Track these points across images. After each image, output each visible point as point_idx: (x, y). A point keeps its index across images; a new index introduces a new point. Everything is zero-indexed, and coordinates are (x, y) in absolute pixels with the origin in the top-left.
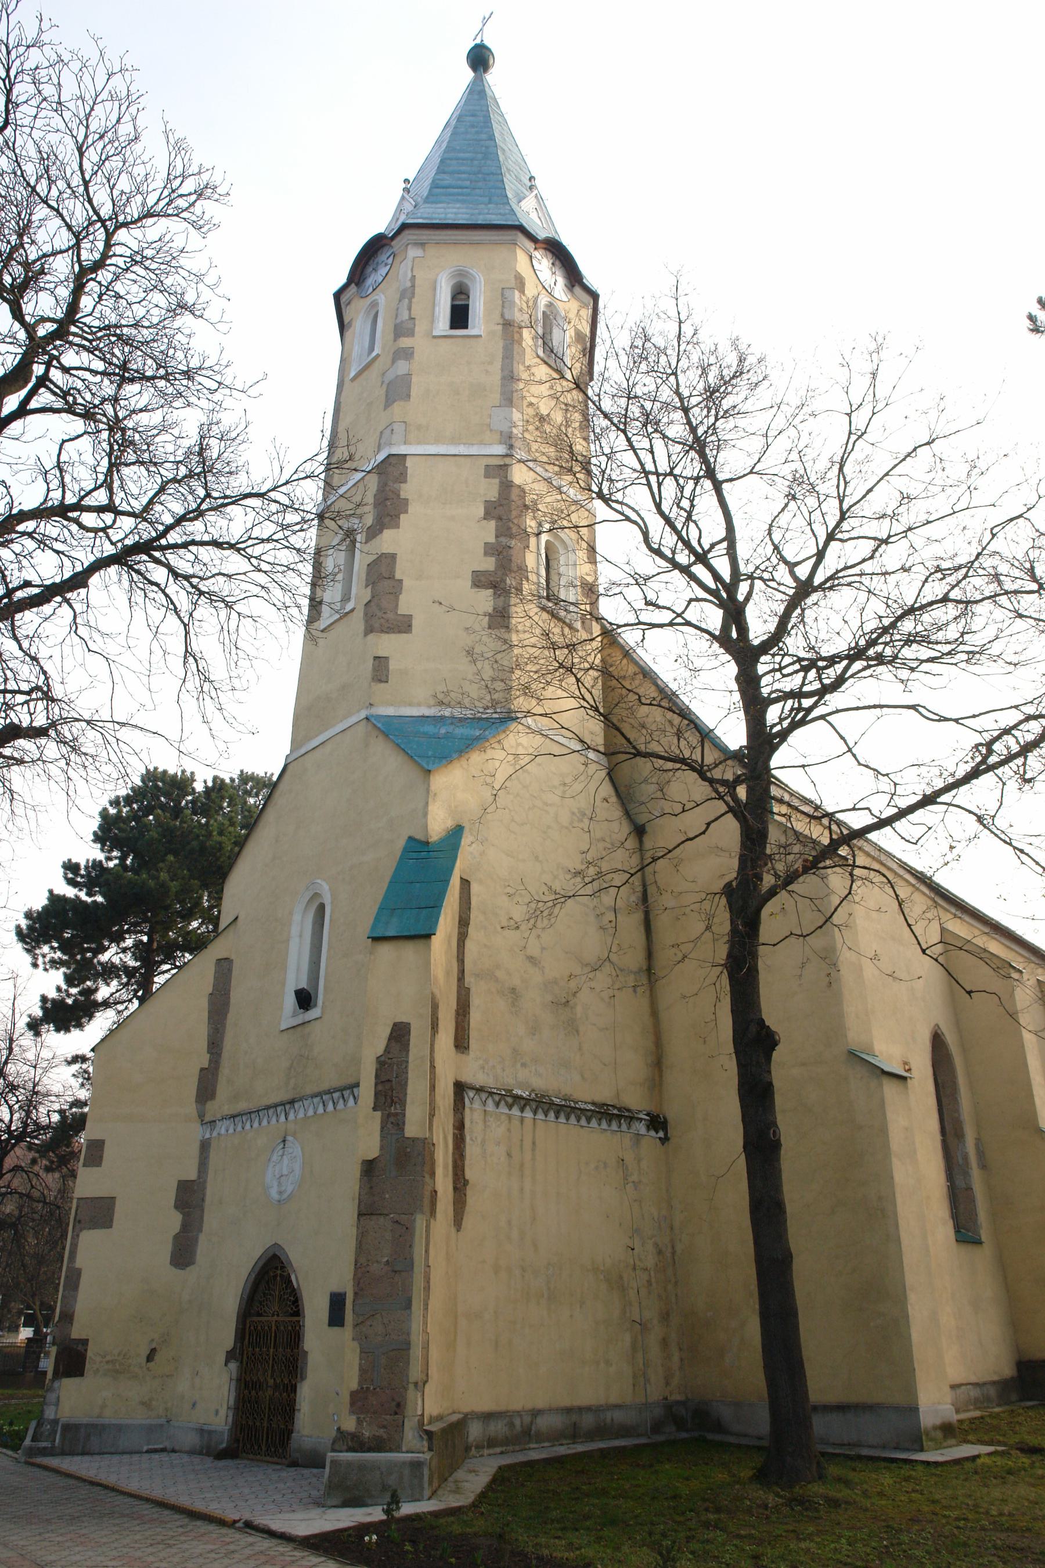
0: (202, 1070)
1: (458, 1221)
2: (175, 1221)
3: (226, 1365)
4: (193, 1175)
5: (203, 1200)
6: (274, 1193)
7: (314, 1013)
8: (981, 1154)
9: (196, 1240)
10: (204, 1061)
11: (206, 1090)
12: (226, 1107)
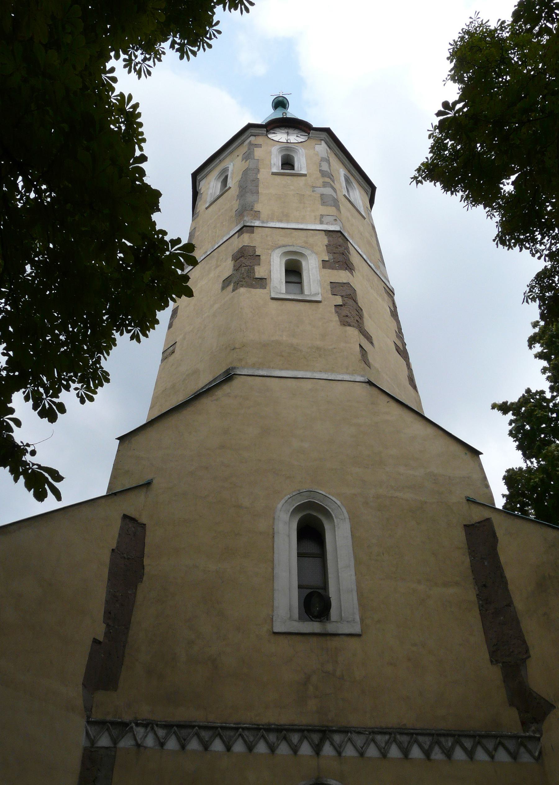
11: (105, 666)
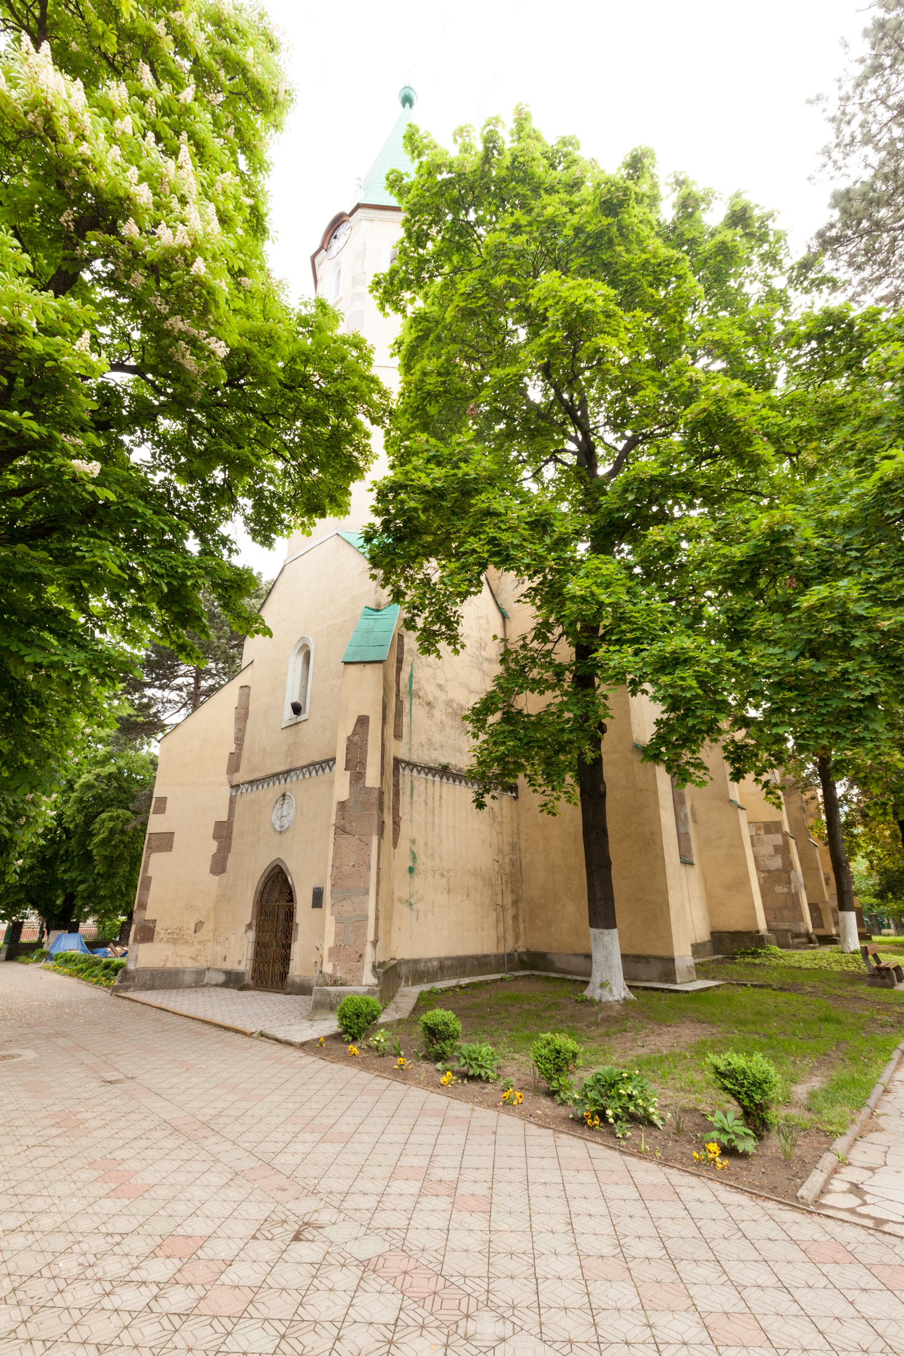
1: (395, 845)
2: (213, 846)
4: (225, 819)
7: (302, 717)
8: (693, 814)
10: (233, 748)
11: (234, 764)
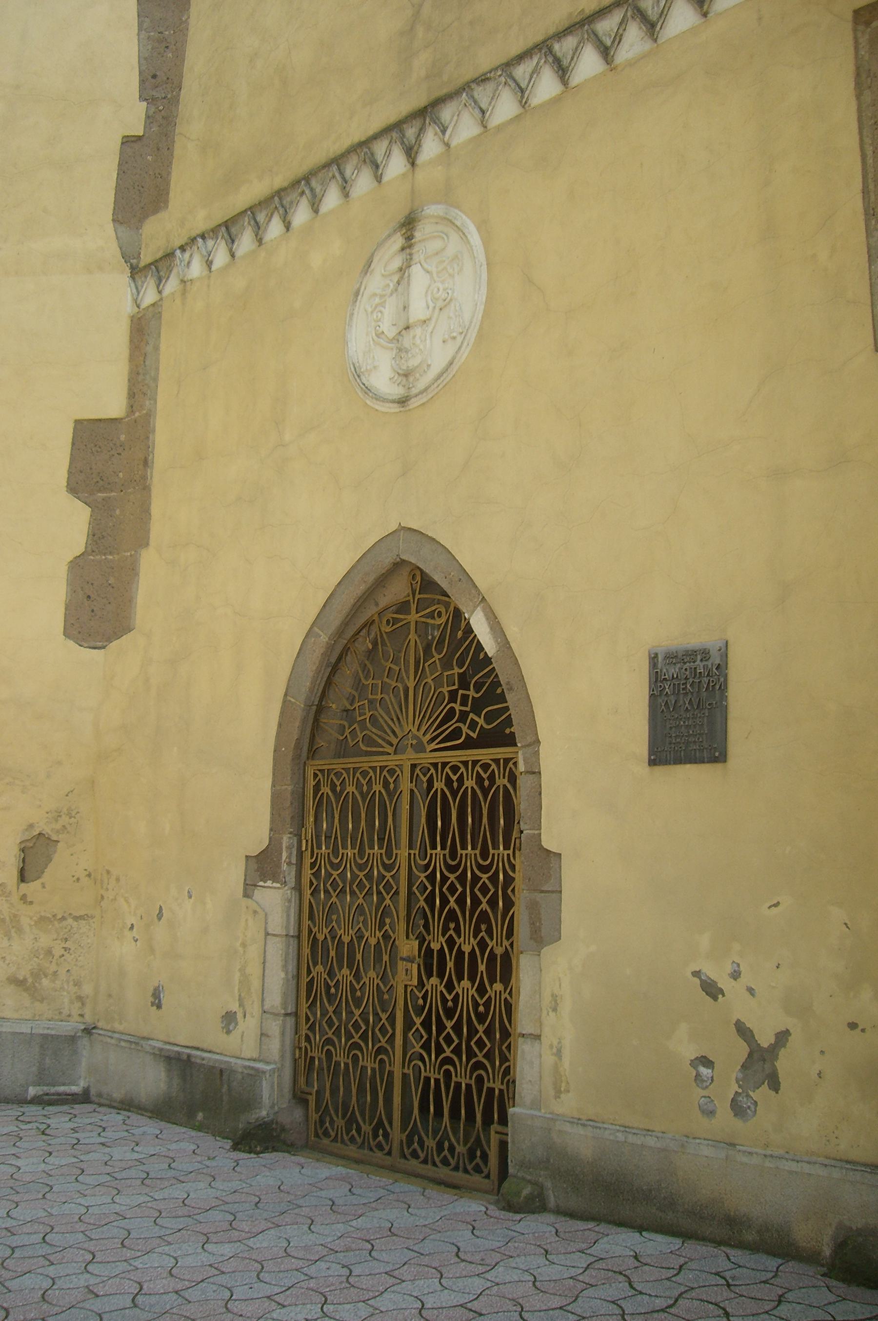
0: (128, 141)
2: (70, 525)
3: (247, 895)
4: (113, 405)
5: (146, 463)
6: (383, 381)
9: (133, 570)
10: (133, 118)
11: (142, 179)
12: (201, 214)
